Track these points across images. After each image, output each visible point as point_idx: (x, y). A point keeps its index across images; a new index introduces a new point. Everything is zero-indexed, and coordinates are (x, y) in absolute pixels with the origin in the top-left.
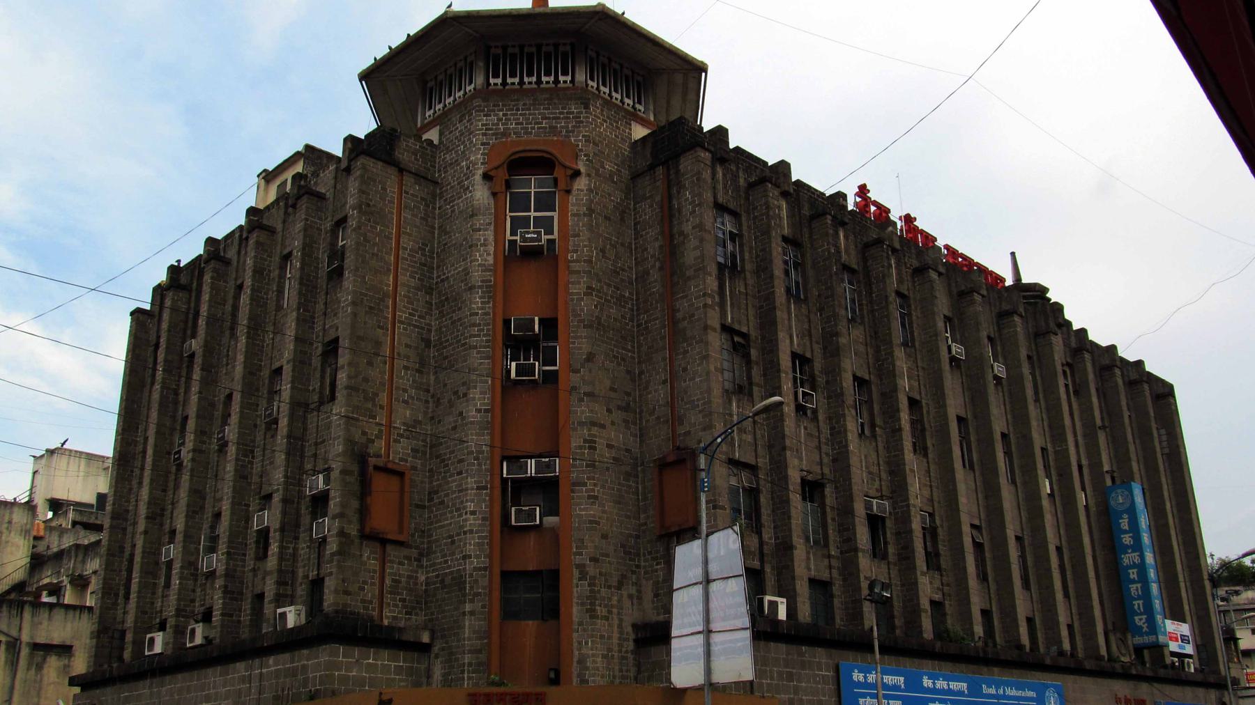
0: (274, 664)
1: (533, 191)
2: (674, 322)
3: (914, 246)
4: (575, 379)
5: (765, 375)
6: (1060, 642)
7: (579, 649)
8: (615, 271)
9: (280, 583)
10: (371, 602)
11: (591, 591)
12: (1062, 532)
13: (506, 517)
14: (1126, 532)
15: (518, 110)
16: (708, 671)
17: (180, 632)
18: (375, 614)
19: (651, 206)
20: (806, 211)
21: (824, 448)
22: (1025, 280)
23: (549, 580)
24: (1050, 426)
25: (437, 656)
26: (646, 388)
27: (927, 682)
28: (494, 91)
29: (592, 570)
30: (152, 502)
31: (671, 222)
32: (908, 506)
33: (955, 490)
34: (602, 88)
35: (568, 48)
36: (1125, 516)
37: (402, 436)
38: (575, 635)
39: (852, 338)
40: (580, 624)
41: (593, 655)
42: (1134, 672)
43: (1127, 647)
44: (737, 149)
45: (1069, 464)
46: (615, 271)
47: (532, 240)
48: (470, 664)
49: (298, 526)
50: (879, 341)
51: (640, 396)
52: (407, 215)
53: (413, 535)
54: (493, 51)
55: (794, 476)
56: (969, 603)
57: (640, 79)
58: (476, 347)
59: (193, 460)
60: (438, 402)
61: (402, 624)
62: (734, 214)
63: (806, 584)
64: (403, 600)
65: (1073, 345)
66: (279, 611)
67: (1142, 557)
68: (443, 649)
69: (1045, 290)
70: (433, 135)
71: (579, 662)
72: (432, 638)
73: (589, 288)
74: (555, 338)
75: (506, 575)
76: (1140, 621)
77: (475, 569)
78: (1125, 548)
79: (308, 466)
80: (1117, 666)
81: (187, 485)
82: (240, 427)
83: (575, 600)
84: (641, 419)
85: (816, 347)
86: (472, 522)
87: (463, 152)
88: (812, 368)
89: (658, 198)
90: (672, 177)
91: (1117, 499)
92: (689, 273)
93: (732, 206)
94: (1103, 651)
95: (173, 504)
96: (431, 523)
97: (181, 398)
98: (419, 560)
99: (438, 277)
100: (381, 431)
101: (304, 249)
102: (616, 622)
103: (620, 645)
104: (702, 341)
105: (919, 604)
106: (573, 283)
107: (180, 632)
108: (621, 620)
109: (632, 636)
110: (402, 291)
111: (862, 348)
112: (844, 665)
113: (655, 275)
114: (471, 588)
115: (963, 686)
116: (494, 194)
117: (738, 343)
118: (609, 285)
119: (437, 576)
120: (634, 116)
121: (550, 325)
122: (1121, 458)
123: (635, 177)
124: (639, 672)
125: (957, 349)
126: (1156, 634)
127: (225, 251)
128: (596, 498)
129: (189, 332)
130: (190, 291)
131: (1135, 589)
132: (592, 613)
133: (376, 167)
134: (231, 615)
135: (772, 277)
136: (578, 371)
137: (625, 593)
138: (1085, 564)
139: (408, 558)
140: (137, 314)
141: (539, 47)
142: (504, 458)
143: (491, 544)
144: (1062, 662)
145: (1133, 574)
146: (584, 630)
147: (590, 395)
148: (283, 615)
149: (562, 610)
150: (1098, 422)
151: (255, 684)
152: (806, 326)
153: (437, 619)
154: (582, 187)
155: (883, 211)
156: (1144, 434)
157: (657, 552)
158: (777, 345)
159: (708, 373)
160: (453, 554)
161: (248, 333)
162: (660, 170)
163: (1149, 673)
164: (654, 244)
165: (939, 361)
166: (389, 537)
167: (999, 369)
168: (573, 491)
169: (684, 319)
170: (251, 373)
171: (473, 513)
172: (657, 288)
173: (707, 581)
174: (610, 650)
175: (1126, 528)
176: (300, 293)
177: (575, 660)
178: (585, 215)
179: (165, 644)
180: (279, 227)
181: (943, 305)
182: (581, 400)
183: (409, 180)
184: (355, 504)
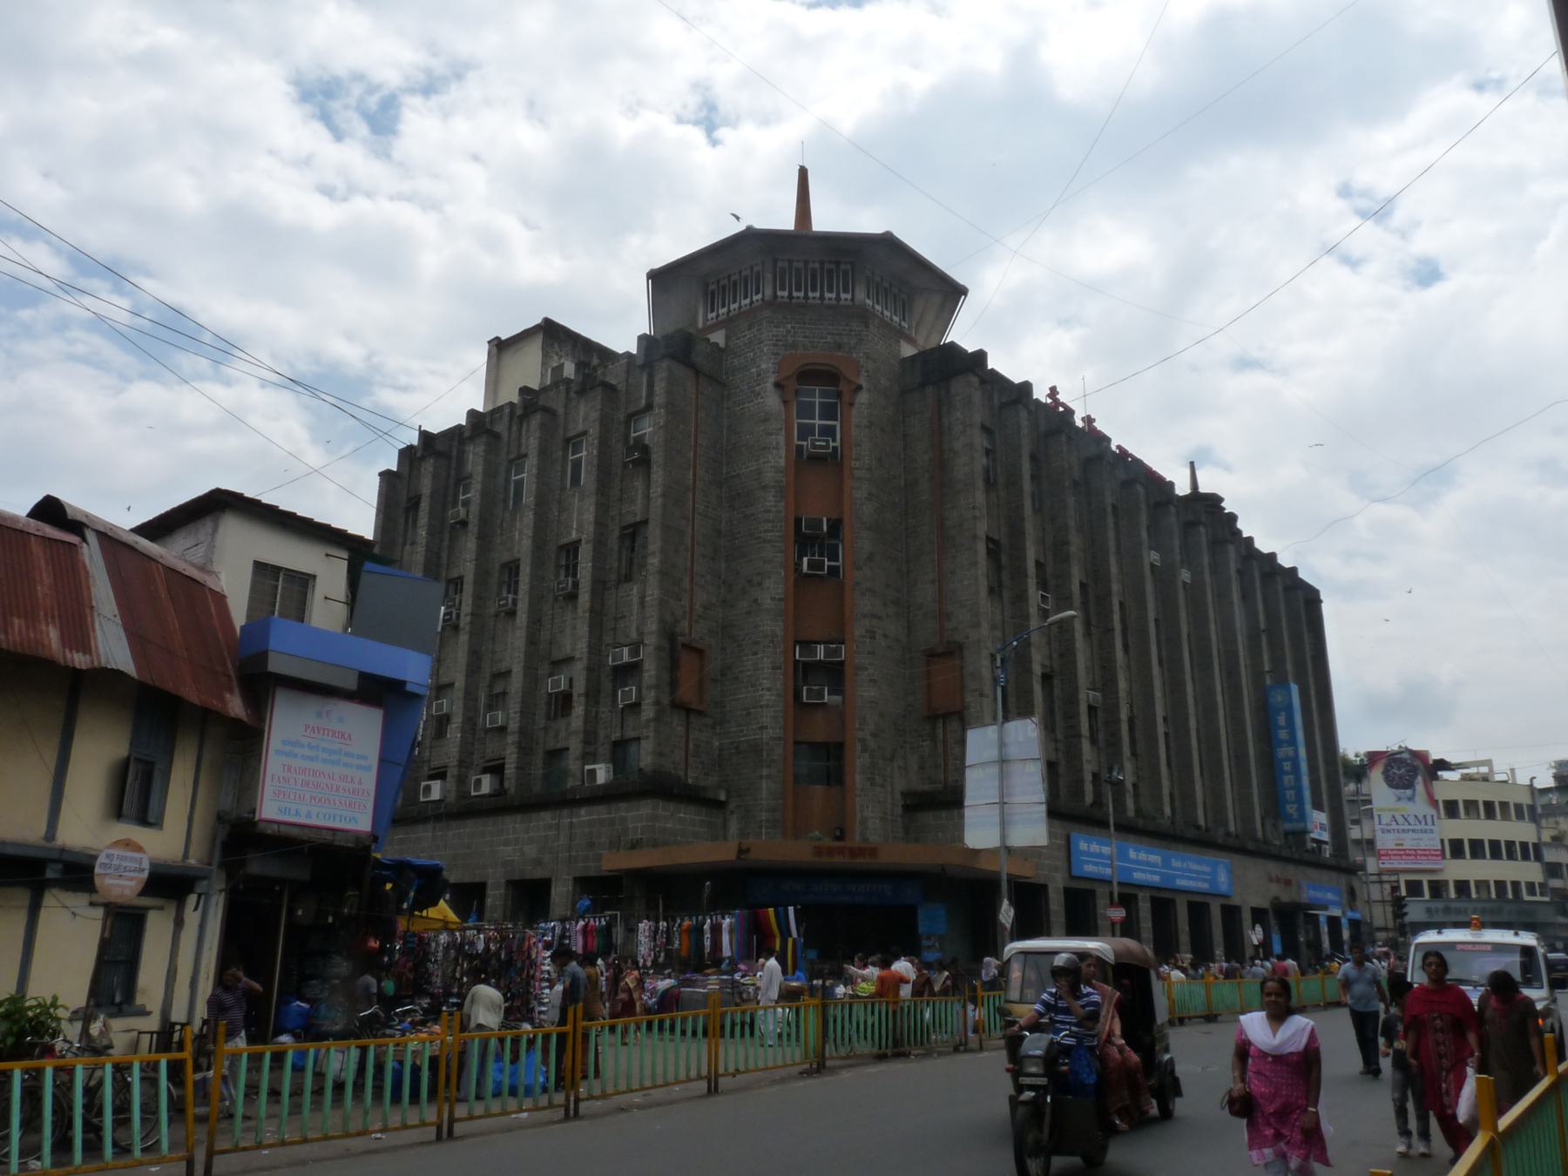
0: (584, 814)
1: (817, 400)
6: (1226, 824)
9: (586, 742)
13: (797, 695)
16: (1003, 836)
17: (462, 780)
18: (682, 774)
22: (1203, 489)
25: (732, 813)
27: (1132, 854)
54: (780, 264)
55: (1037, 669)
59: (471, 623)
67: (1296, 752)
72: (728, 797)
74: (837, 537)
76: (1291, 809)
86: (768, 697)
91: (1277, 698)
94: (1260, 834)
107: (462, 780)
109: (901, 803)
112: (1073, 835)
116: (785, 402)
121: (836, 526)
122: (1278, 661)
127: (492, 422)
128: (875, 681)
131: (1288, 780)
136: (859, 568)
140: (386, 476)
142: (796, 642)
145: (1287, 766)
148: (593, 773)
150: (1262, 626)
155: (1069, 412)
162: (930, 390)
163: (1296, 856)
167: (1185, 575)
171: (769, 689)
173: (1003, 761)
179: (443, 789)
180: (561, 411)
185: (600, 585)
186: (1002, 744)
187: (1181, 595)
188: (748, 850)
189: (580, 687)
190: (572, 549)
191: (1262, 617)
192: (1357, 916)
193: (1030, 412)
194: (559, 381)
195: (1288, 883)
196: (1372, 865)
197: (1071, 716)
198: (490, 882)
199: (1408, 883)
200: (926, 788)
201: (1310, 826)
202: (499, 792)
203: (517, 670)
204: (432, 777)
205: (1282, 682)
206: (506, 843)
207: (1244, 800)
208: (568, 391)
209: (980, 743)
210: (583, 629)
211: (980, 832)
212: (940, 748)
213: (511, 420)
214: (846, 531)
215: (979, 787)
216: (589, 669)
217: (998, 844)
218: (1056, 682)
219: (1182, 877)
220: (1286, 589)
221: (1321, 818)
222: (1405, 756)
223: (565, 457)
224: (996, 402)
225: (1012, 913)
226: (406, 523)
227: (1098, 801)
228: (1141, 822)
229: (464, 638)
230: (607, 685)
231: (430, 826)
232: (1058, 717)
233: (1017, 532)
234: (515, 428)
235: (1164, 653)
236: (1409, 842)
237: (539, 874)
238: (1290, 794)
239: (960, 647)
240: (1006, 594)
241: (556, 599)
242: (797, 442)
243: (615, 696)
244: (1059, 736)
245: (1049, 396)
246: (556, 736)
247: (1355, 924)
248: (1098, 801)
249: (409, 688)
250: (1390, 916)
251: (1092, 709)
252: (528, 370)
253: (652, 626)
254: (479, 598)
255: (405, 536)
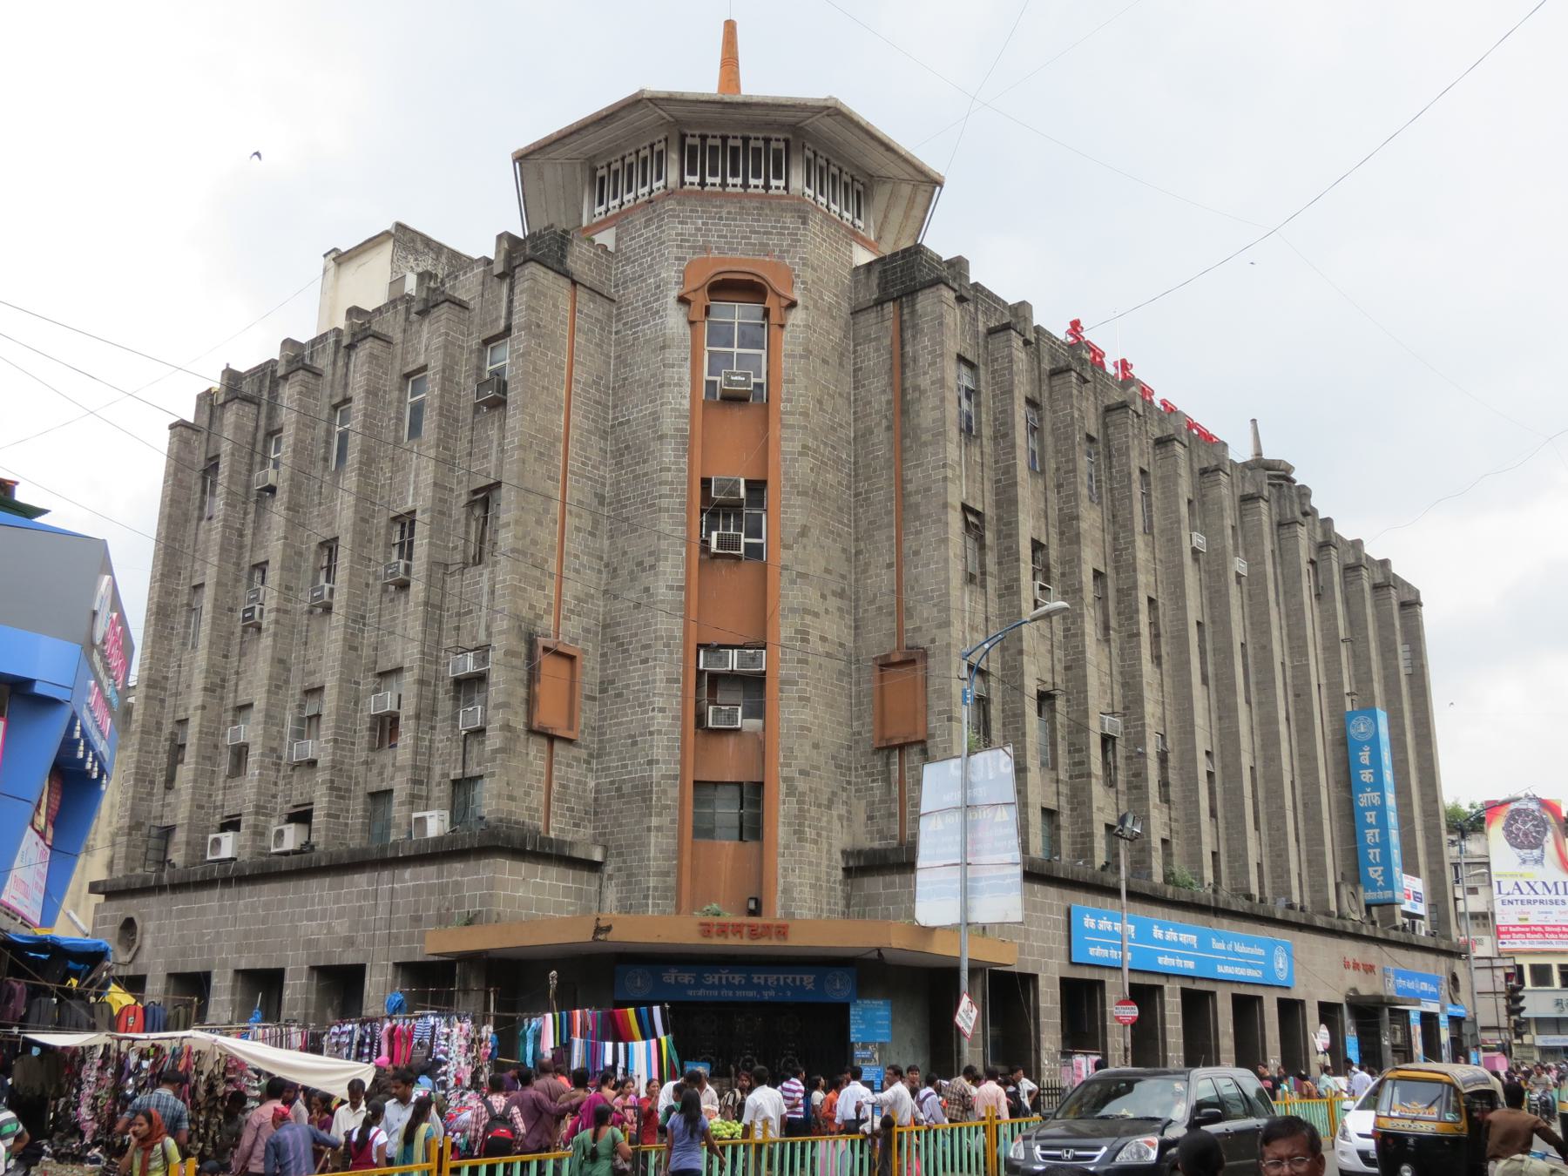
2: (902, 494)
3: (1124, 401)
4: (785, 556)
5: (1000, 563)
6: (1289, 893)
7: (785, 877)
8: (833, 428)
9: (416, 782)
10: (537, 810)
11: (800, 810)
12: (1296, 764)
13: (700, 718)
14: (1366, 767)
15: (721, 218)
16: (965, 909)
17: (259, 832)
18: (541, 824)
19: (877, 350)
20: (1047, 366)
21: (1056, 651)
23: (753, 794)
24: (1289, 636)
25: (610, 877)
26: (865, 571)
27: (1157, 933)
28: (691, 192)
29: (802, 785)
30: (211, 670)
31: (903, 373)
32: (1143, 725)
33: (1191, 708)
34: (819, 198)
35: (782, 145)
36: (1367, 748)
37: (572, 612)
38: (780, 860)
39: (1091, 519)
40: (787, 847)
41: (801, 885)
42: (1365, 932)
43: (1357, 902)
44: (976, 285)
45: (1309, 684)
46: (833, 428)
47: (738, 383)
48: (656, 889)
49: (434, 713)
50: (1118, 523)
51: (857, 580)
52: (580, 338)
53: (583, 732)
54: (689, 141)
56: (1200, 843)
57: (861, 188)
58: (667, 510)
59: (277, 622)
60: (614, 573)
61: (569, 838)
62: (971, 365)
63: (1039, 813)
64: (571, 810)
65: (1319, 539)
66: (415, 815)
67: (1383, 797)
68: (619, 869)
69: (1290, 469)
70: (606, 238)
71: (785, 891)
72: (605, 856)
73: (804, 447)
75: (698, 784)
76: (1375, 873)
77: (664, 777)
78: (1363, 787)
79: (448, 642)
80: (1349, 924)
81: (269, 652)
82: (350, 586)
83: (781, 819)
84: (856, 608)
85: (1051, 530)
86: (660, 721)
87: (651, 266)
88: (1047, 556)
89: (887, 342)
90: (906, 317)
91: (1358, 729)
92: (925, 437)
93: (969, 357)
94: (1333, 907)
95: (237, 673)
96: (605, 719)
97: (248, 540)
98: (588, 763)
99: (615, 418)
100: (549, 604)
101: (444, 371)
102: (825, 846)
103: (828, 874)
104: (939, 520)
105: (1149, 842)
106: (786, 439)
107: (259, 832)
108: (830, 845)
110: (574, 434)
111: (1098, 534)
113: (880, 436)
114: (659, 799)
115: (1191, 939)
116: (692, 323)
117: (973, 521)
118: (825, 444)
119: (612, 783)
120: (854, 235)
122: (1363, 679)
123: (855, 313)
124: (848, 906)
125: (1199, 540)
126: (1392, 889)
128: (807, 700)
129: (258, 458)
130: (259, 405)
131: (1371, 835)
132: (799, 834)
133: (546, 278)
134: (337, 817)
135: (1013, 446)
137: (835, 813)
138: (1319, 803)
139: (577, 759)
140: (179, 427)
141: (746, 140)
143: (683, 749)
144: (1293, 916)
145: (1371, 817)
146: (792, 855)
147: (801, 575)
148: (422, 821)
149: (766, 829)
150: (1342, 635)
151: (383, 902)
152: (1042, 506)
153: (612, 833)
154: (799, 322)
155: (1098, 354)
156: (1388, 650)
157: (874, 766)
158: (1017, 528)
159: (946, 560)
160: (635, 757)
161: (360, 469)
162: (890, 307)
163: (1380, 935)
164: (879, 395)
165: (1181, 553)
166: (558, 733)
167: (1239, 565)
168: (781, 691)
169: (917, 492)
170: (363, 520)
171: (662, 710)
172: (882, 451)
173: (968, 807)
174: (818, 879)
175: (1367, 762)
176: (439, 427)
177: (780, 889)
178: (801, 357)
180: (397, 337)
181: (1185, 489)
182: (793, 582)
183: (582, 295)
184: (521, 692)
185: (440, 568)
186: (966, 784)
187: (1234, 589)
188: (609, 929)
189: (408, 709)
190: (406, 522)
191: (1341, 623)
192: (1458, 1012)
193: (1027, 343)
194: (398, 300)
195: (1369, 969)
196: (1484, 947)
197: (1078, 749)
198: (288, 970)
199: (1533, 968)
200: (876, 845)
201: (1399, 896)
202: (307, 847)
203: (331, 684)
204: (224, 828)
205: (1368, 710)
206: (311, 916)
207: (1315, 861)
208: (408, 310)
209: (938, 783)
210: (415, 627)
211: (935, 902)
212: (896, 789)
213: (336, 353)
214: (771, 493)
215: (935, 843)
216: (421, 682)
217: (957, 920)
218: (1060, 704)
219: (1223, 963)
220: (1376, 587)
221: (1416, 884)
222: (1533, 806)
223: (401, 401)
224: (982, 328)
225: (975, 1013)
226: (204, 491)
227: (1112, 865)
228: (1170, 891)
229: (266, 641)
230: (445, 705)
231: (217, 892)
232: (1062, 749)
233: (1006, 497)
234: (340, 363)
235: (1210, 669)
236: (1535, 916)
237: (349, 958)
238: (1374, 854)
239: (925, 654)
240: (992, 583)
241: (385, 590)
242: (706, 376)
243: (455, 718)
244: (1063, 776)
245: (1069, 333)
246: (381, 774)
247: (1456, 1021)
248: (1112, 865)
249: (39, 689)
250: (1503, 1012)
251: (1107, 740)
252: (370, 286)
253: (502, 624)
254: (287, 589)
255: (201, 508)
